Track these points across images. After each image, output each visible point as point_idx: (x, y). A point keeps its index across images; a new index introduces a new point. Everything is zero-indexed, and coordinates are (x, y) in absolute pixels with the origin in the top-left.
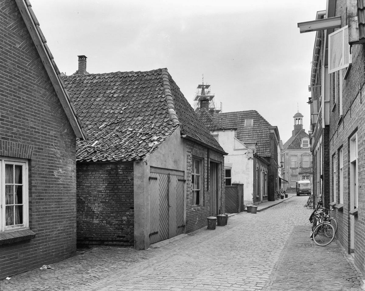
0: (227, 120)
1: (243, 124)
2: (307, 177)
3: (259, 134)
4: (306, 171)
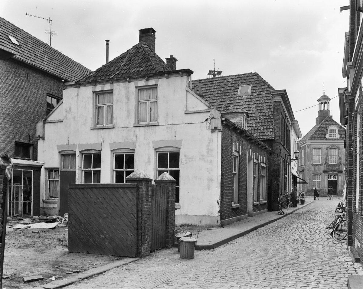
0: (213, 87)
1: (236, 93)
2: (334, 176)
3: (259, 105)
4: (333, 169)
